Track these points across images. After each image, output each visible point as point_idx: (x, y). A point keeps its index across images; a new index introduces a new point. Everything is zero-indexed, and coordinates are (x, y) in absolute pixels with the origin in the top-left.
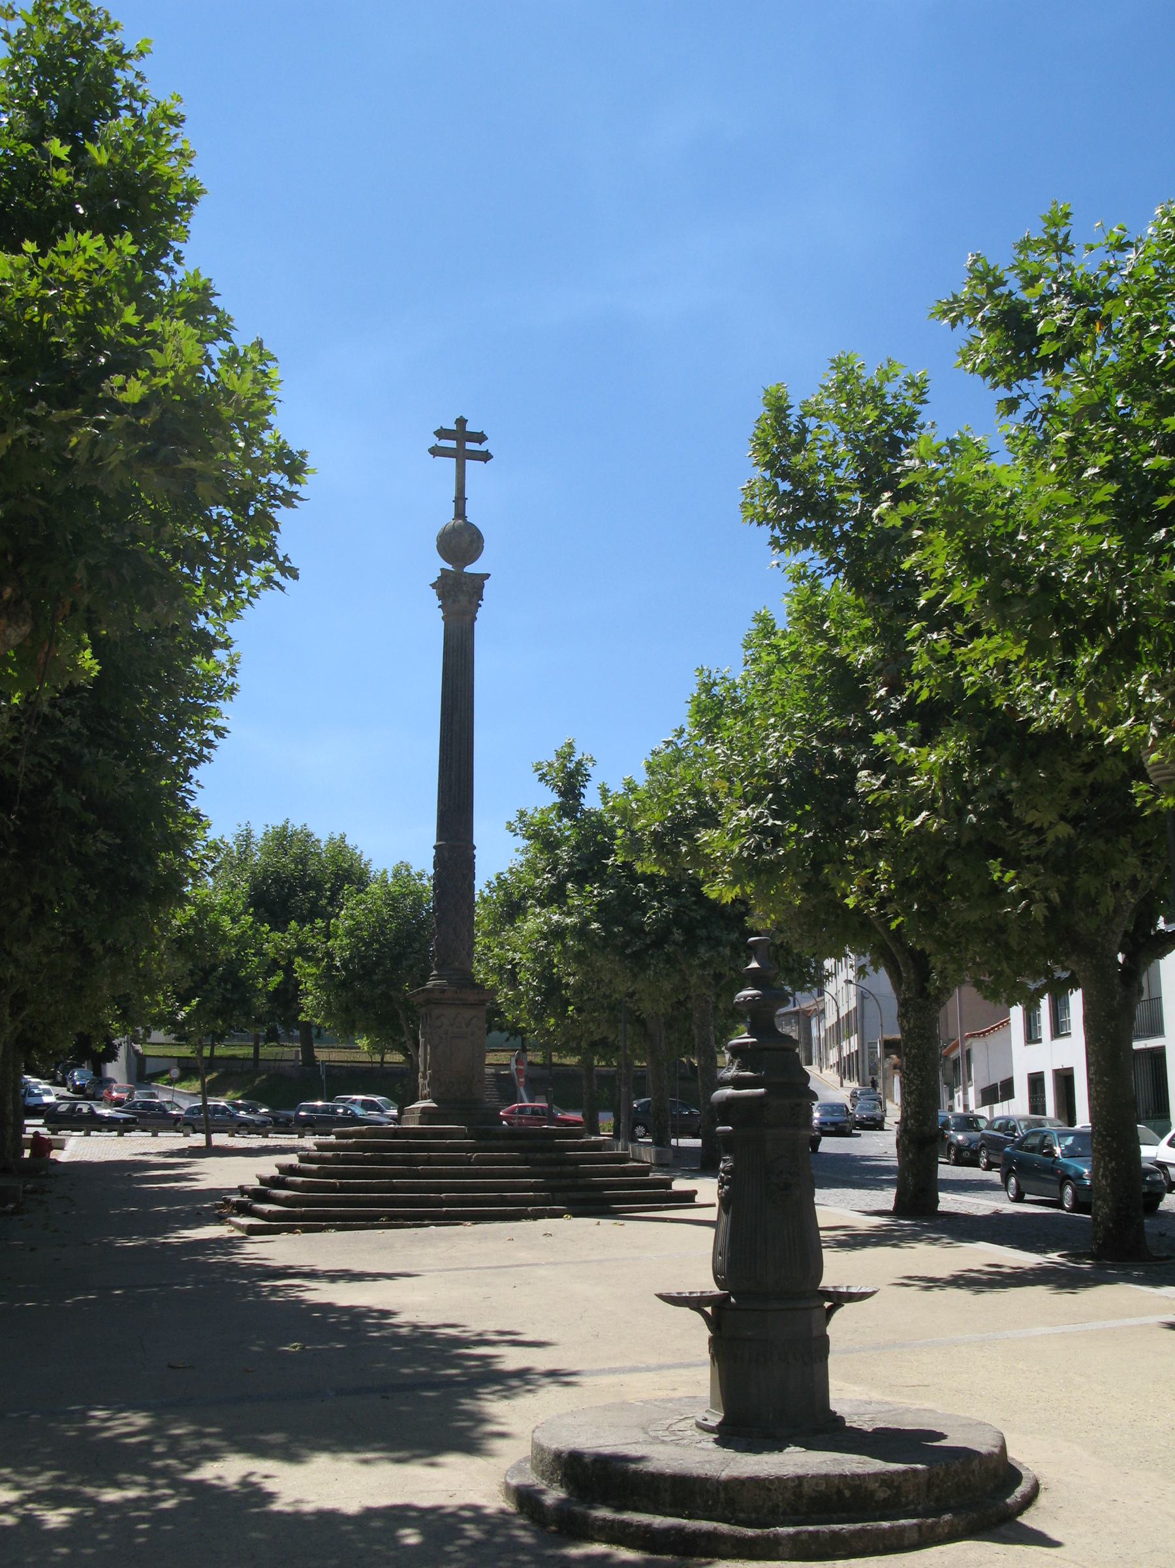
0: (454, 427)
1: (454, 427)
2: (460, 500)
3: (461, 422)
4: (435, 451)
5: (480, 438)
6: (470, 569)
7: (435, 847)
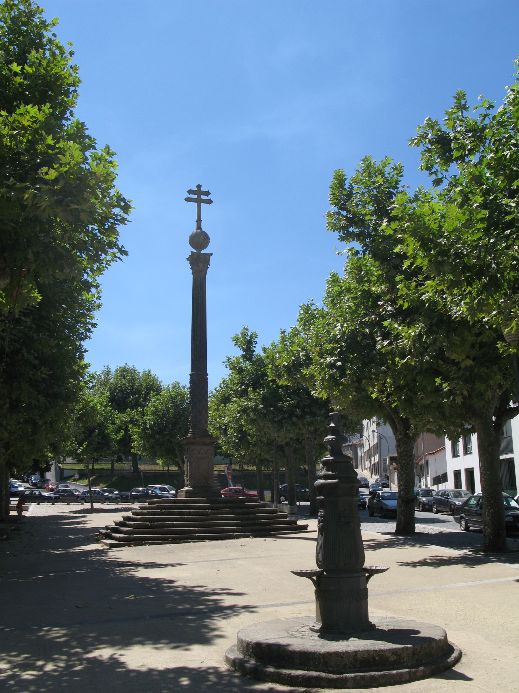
0: (196, 189)
1: (196, 189)
2: (199, 221)
3: (199, 186)
4: (188, 200)
5: (207, 193)
6: (204, 251)
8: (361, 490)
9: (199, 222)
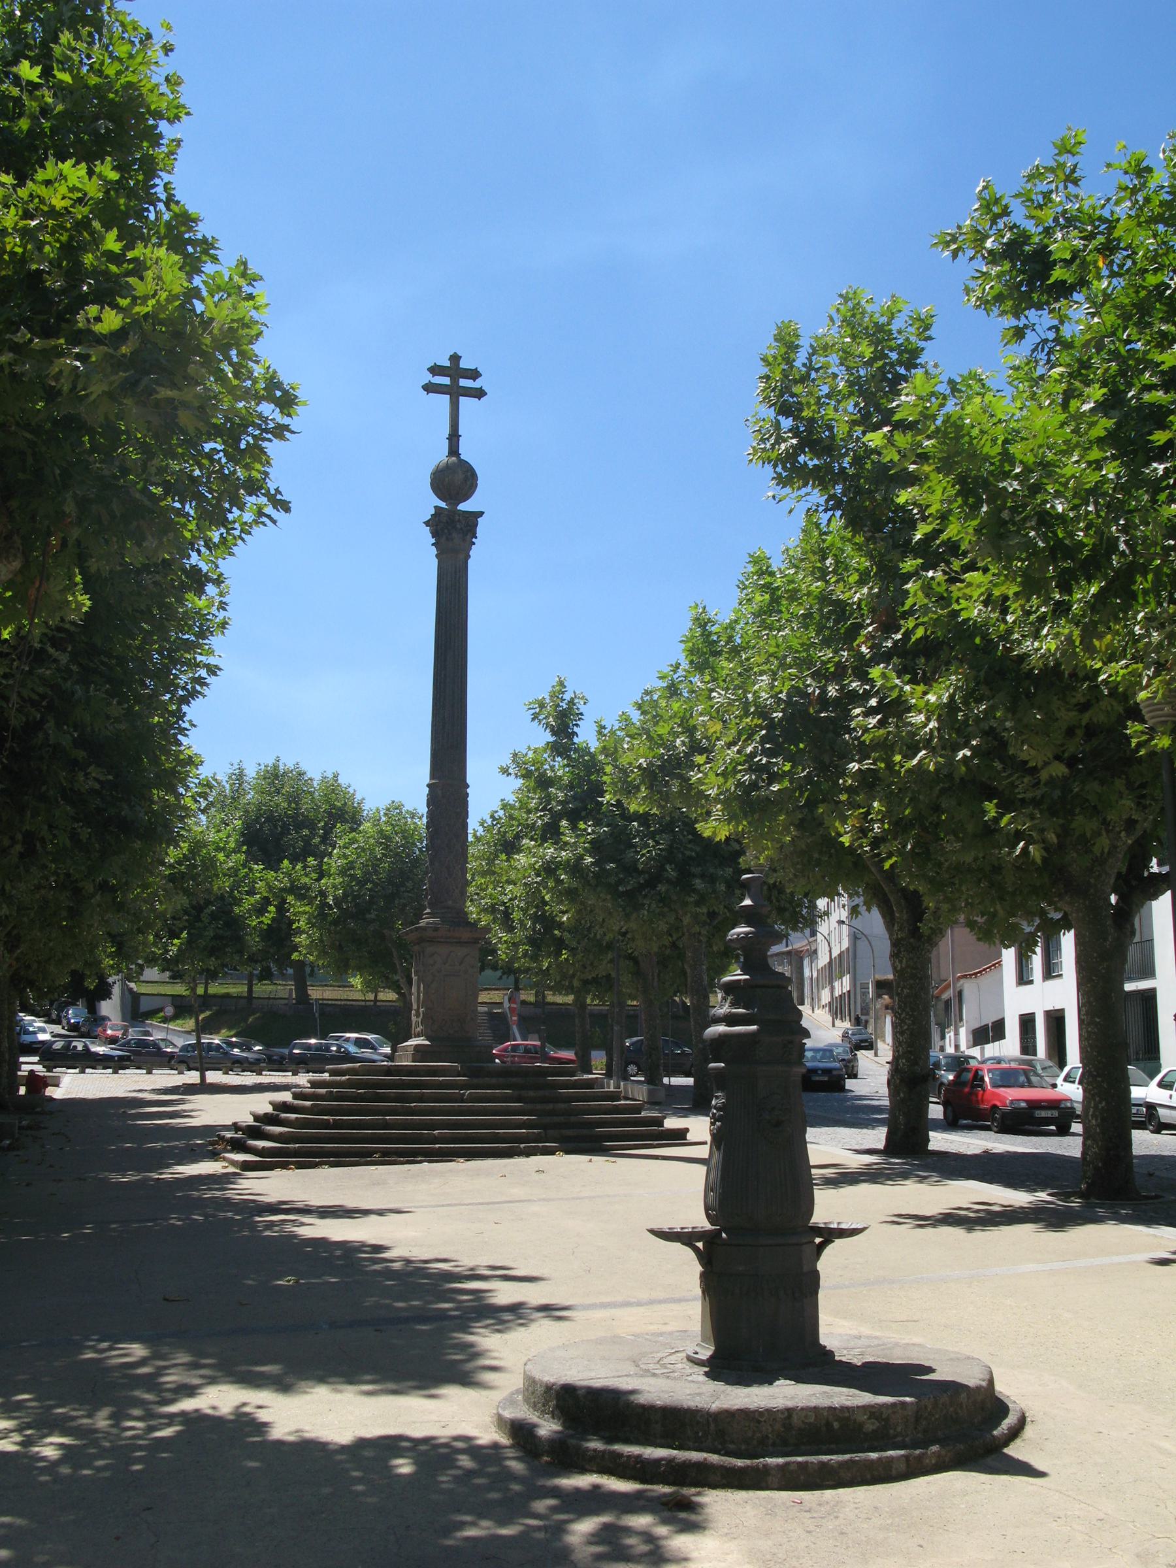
0: (448, 364)
1: (448, 364)
2: (454, 437)
3: (455, 358)
4: (429, 388)
5: (474, 374)
6: (463, 507)
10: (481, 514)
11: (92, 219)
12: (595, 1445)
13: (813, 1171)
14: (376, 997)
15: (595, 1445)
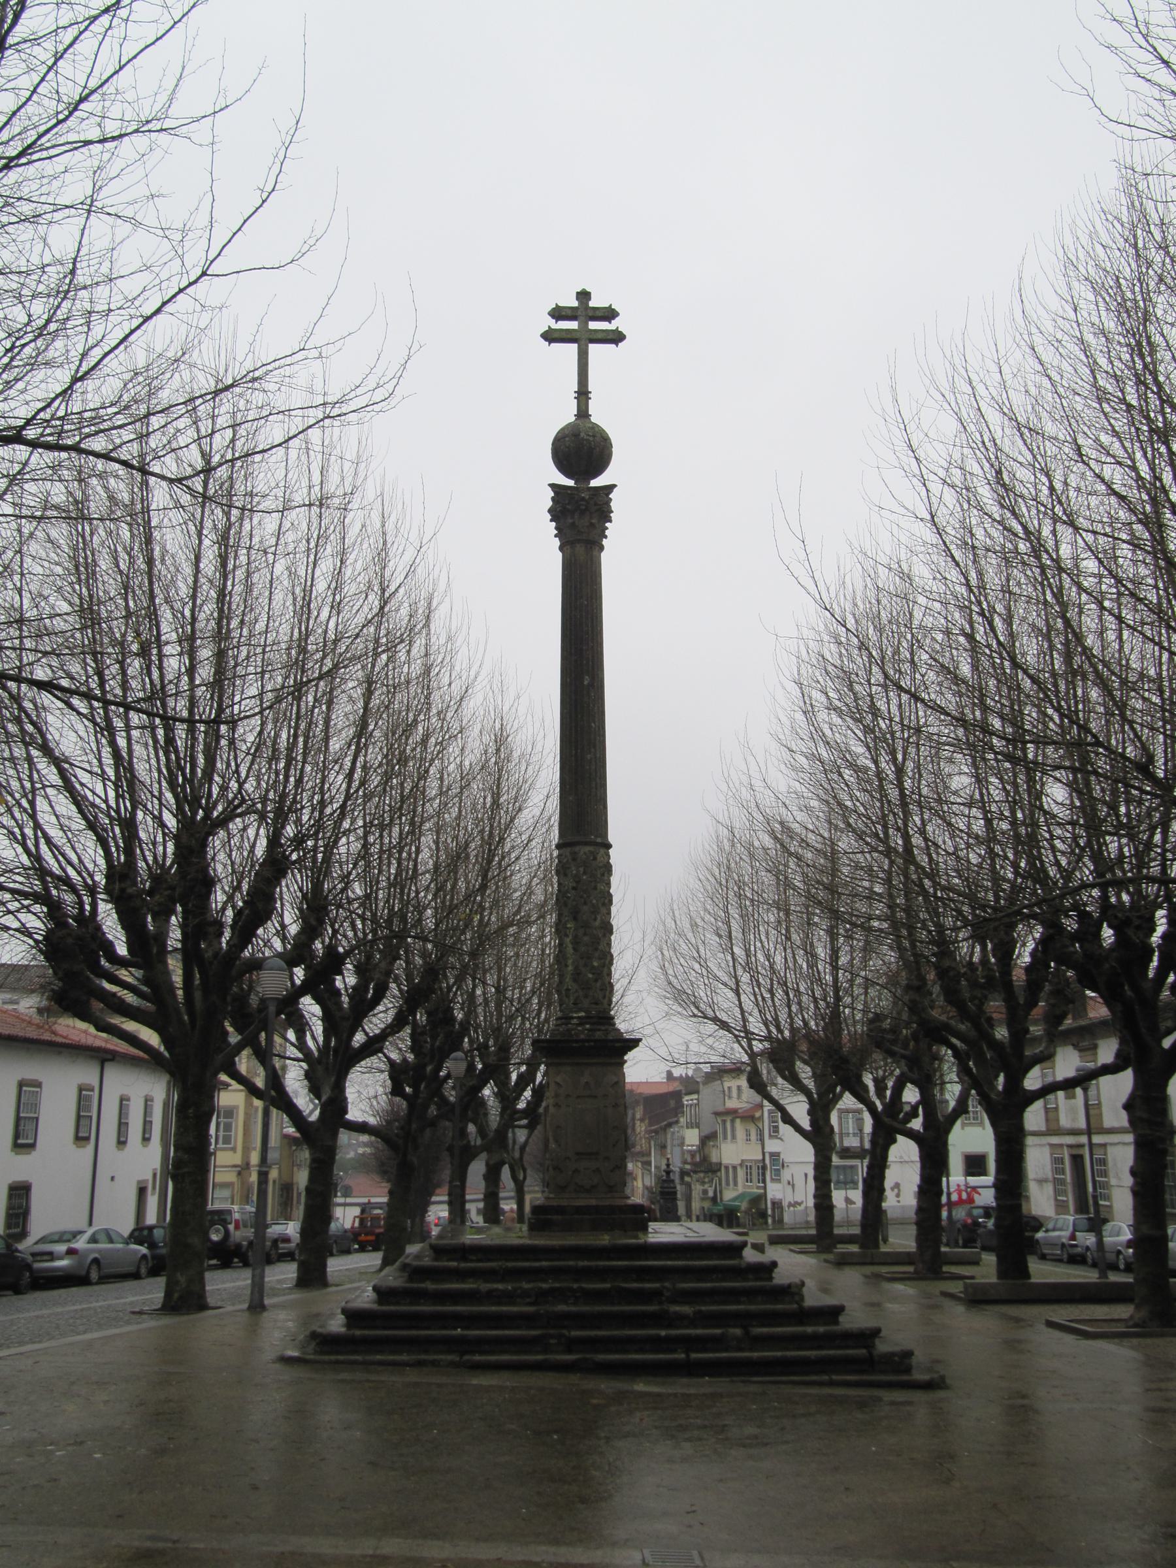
0: (575, 304)
1: (575, 304)
2: (583, 394)
3: (584, 296)
4: (550, 337)
5: (609, 314)
6: (595, 483)
7: (606, 537)
8: (298, 982)
9: (583, 398)
10: (614, 486)
11: (911, 1134)
12: (990, 946)
13: (446, 1198)
14: (182, 720)
15: (990, 946)
